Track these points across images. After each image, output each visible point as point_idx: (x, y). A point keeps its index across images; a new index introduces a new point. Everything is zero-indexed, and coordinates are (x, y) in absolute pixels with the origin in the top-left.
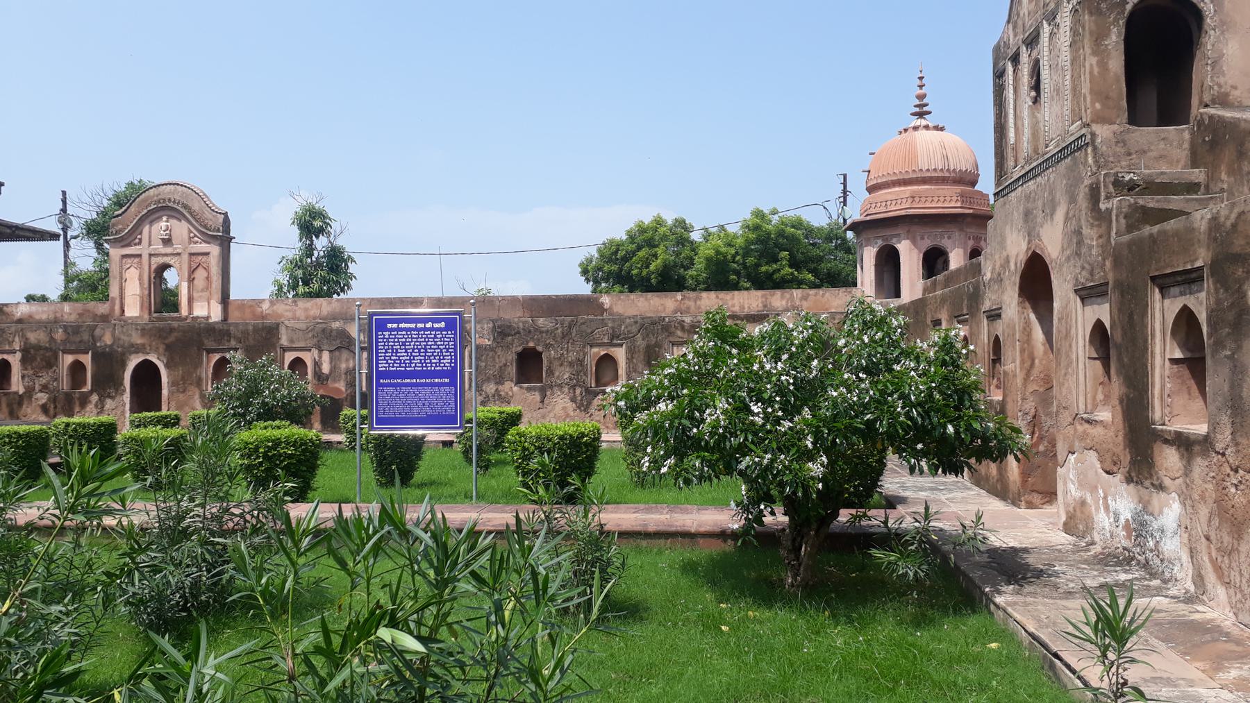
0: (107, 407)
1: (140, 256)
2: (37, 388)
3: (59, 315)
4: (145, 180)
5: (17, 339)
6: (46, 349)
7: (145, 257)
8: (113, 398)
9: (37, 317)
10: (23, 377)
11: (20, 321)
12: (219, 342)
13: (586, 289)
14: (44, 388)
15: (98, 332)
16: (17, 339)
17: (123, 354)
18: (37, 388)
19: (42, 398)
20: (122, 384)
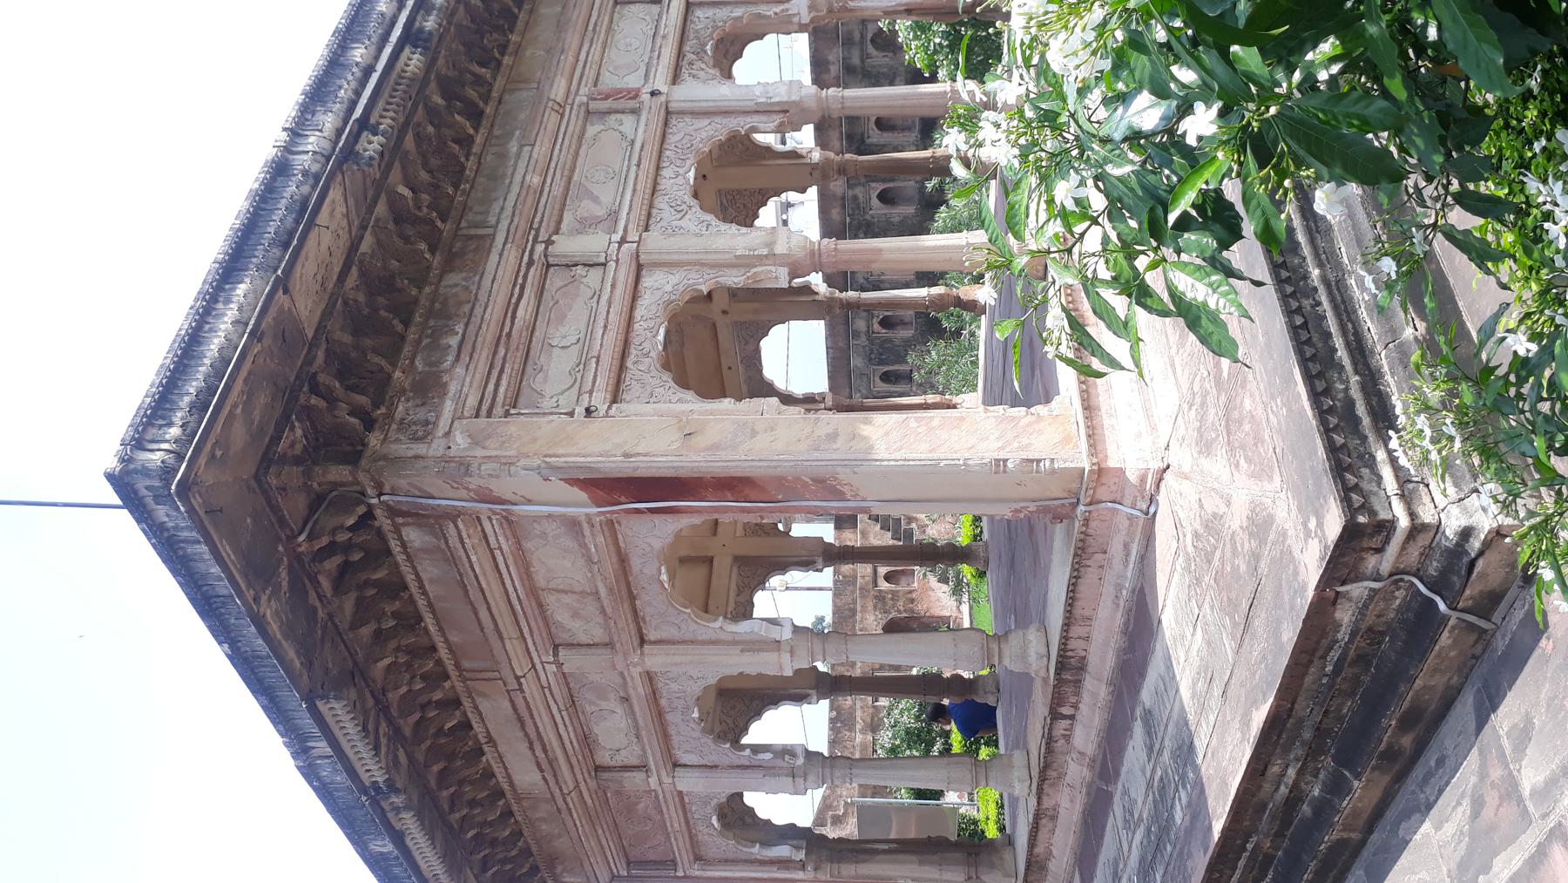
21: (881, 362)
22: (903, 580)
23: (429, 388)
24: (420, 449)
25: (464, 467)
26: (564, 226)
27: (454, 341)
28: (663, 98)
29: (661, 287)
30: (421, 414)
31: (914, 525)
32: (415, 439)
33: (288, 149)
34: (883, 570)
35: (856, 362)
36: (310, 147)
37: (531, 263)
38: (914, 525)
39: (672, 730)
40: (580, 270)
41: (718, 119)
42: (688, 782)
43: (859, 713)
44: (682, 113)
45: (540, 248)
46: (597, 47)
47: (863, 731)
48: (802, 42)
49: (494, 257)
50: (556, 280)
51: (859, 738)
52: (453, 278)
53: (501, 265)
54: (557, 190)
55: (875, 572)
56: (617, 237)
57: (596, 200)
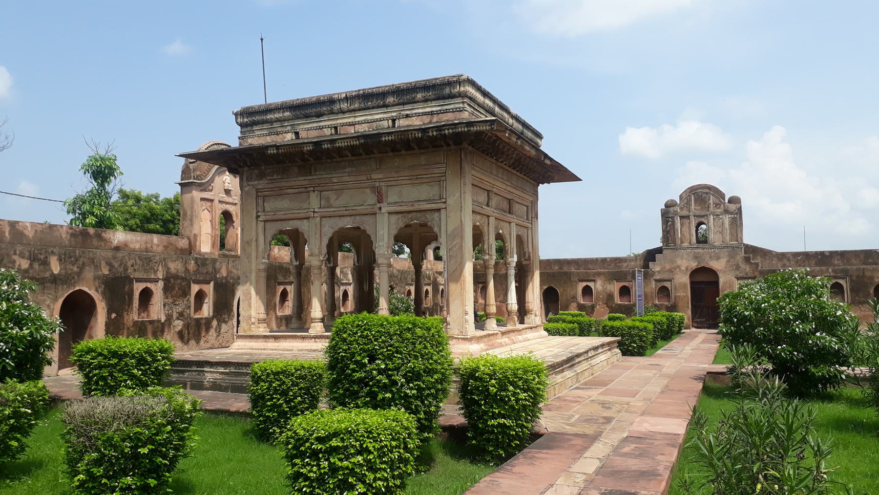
0: (223, 330)
1: (212, 201)
2: (175, 315)
3: (149, 246)
4: (235, 111)
5: (160, 268)
6: (182, 278)
7: (216, 202)
8: (226, 322)
9: (132, 246)
10: (164, 305)
11: (117, 249)
12: (285, 277)
13: (118, 227)
14: (181, 315)
15: (218, 265)
16: (160, 268)
17: (233, 285)
18: (175, 315)
19: (178, 324)
20: (232, 310)
23: (261, 176)
27: (275, 177)
30: (254, 176)
32: (247, 179)
39: (276, 223)
46: (408, 182)
49: (303, 178)
52: (296, 170)
53: (302, 181)
57: (337, 199)
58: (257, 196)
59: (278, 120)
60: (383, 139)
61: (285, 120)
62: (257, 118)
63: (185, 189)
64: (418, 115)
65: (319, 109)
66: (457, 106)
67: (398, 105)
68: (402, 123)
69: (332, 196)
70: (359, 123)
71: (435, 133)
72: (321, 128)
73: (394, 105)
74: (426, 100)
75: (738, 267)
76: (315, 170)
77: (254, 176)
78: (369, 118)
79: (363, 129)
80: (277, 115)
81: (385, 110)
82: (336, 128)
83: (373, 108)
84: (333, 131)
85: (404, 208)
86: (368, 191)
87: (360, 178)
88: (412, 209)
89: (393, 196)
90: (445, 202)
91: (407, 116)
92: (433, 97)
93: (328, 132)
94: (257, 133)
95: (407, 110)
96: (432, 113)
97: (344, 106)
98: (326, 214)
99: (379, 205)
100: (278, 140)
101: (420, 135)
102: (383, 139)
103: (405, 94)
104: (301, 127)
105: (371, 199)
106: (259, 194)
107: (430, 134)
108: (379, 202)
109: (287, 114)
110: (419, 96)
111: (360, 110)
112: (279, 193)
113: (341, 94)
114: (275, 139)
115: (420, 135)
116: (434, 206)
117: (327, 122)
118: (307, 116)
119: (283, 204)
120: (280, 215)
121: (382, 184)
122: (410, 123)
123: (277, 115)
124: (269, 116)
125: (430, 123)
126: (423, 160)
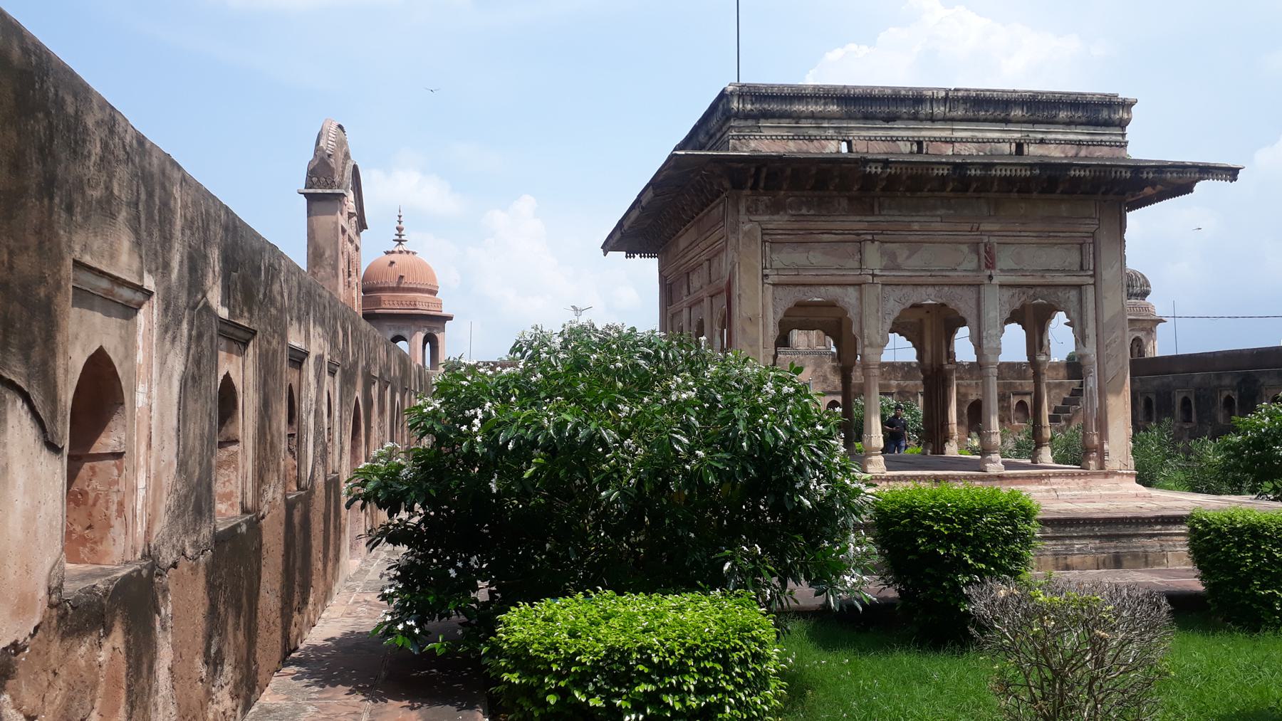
21: (1197, 398)
22: (1020, 415)
23: (776, 208)
24: (743, 210)
25: (735, 230)
26: (887, 245)
27: (804, 211)
28: (986, 281)
29: (849, 298)
30: (761, 207)
31: (1063, 423)
32: (748, 210)
33: (932, 100)
34: (1028, 400)
35: (1198, 377)
36: (935, 109)
37: (858, 235)
38: (1063, 423)
40: (857, 257)
41: (975, 311)
42: (685, 313)
43: (911, 383)
44: (979, 293)
45: (870, 237)
46: (1035, 240)
47: (898, 385)
48: (974, 359)
49: (858, 218)
50: (851, 248)
51: (894, 383)
52: (844, 203)
53: (856, 222)
54: (910, 238)
55: (1026, 394)
56: (877, 272)
57: (908, 257)
58: (764, 242)
59: (812, 116)
60: (1072, 173)
61: (824, 118)
62: (774, 107)
63: (316, 205)
64: (1059, 142)
65: (893, 109)
66: (1114, 138)
67: (1025, 122)
68: (1033, 150)
69: (902, 253)
70: (962, 141)
71: (1151, 175)
72: (894, 140)
73: (1018, 122)
74: (1070, 123)
75: (825, 379)
76: (881, 206)
77: (761, 207)
78: (979, 135)
79: (968, 150)
80: (812, 108)
81: (912, 125)
82: (920, 143)
83: (985, 120)
84: (915, 148)
85: (1029, 280)
86: (965, 248)
87: (959, 227)
88: (1041, 281)
89: (1005, 259)
90: (1093, 276)
91: (1042, 141)
92: (1083, 119)
93: (905, 147)
94: (766, 133)
95: (1038, 132)
96: (1079, 143)
97: (939, 110)
98: (889, 280)
99: (988, 272)
100: (812, 149)
101: (879, 170)
102: (1072, 173)
103: (1041, 108)
104: (855, 133)
105: (970, 262)
106: (766, 238)
107: (1145, 175)
108: (988, 267)
109: (834, 108)
110: (1063, 115)
111: (962, 120)
112: (803, 240)
113: (938, 89)
114: (805, 148)
115: (1129, 175)
116: (1075, 280)
117: (901, 131)
118: (867, 117)
119: (816, 257)
120: (807, 277)
121: (993, 239)
122: (1046, 153)
123: (812, 108)
124: (798, 107)
125: (1076, 156)
126: (1064, 209)
